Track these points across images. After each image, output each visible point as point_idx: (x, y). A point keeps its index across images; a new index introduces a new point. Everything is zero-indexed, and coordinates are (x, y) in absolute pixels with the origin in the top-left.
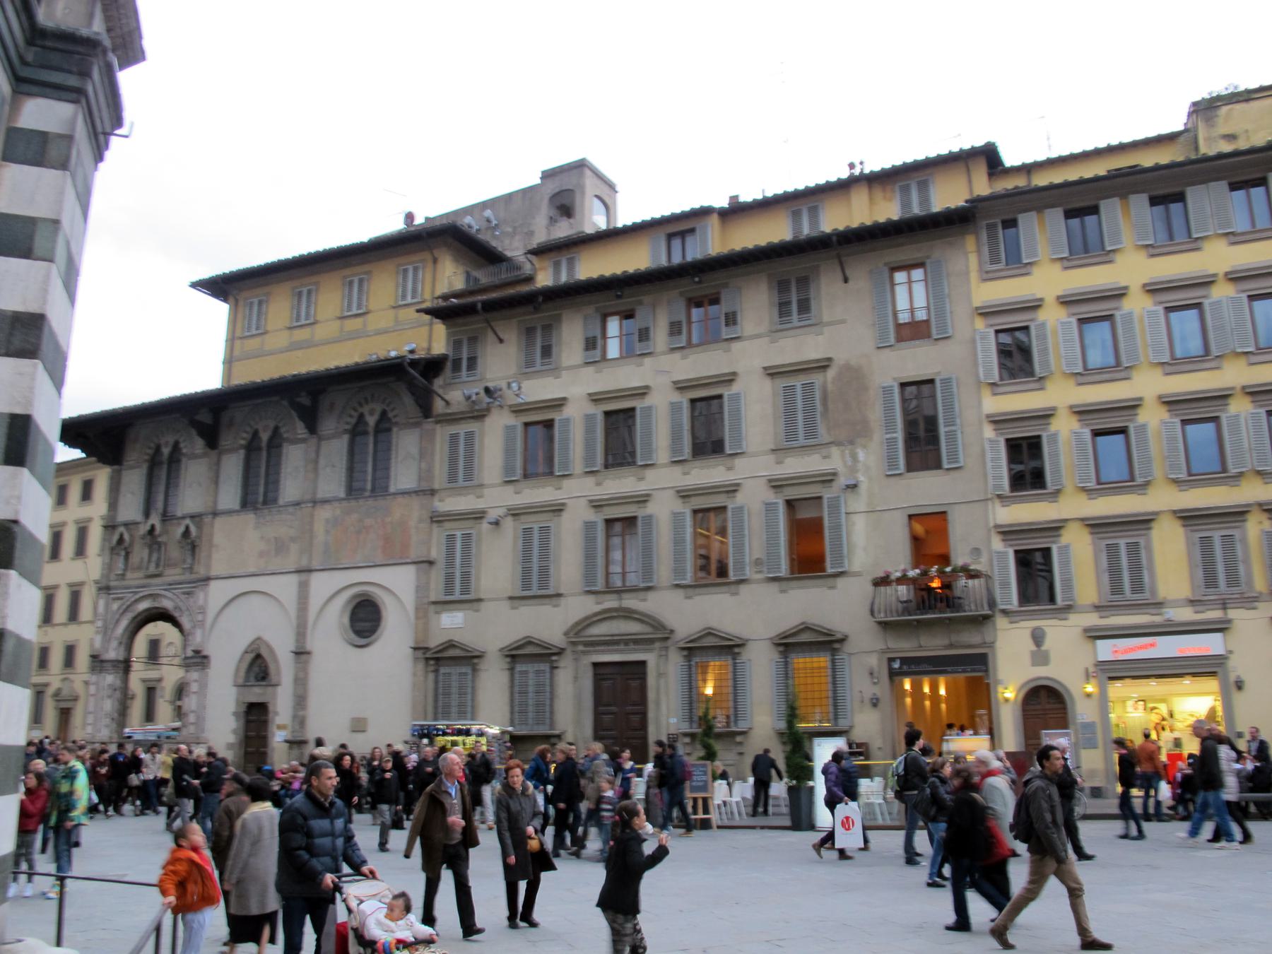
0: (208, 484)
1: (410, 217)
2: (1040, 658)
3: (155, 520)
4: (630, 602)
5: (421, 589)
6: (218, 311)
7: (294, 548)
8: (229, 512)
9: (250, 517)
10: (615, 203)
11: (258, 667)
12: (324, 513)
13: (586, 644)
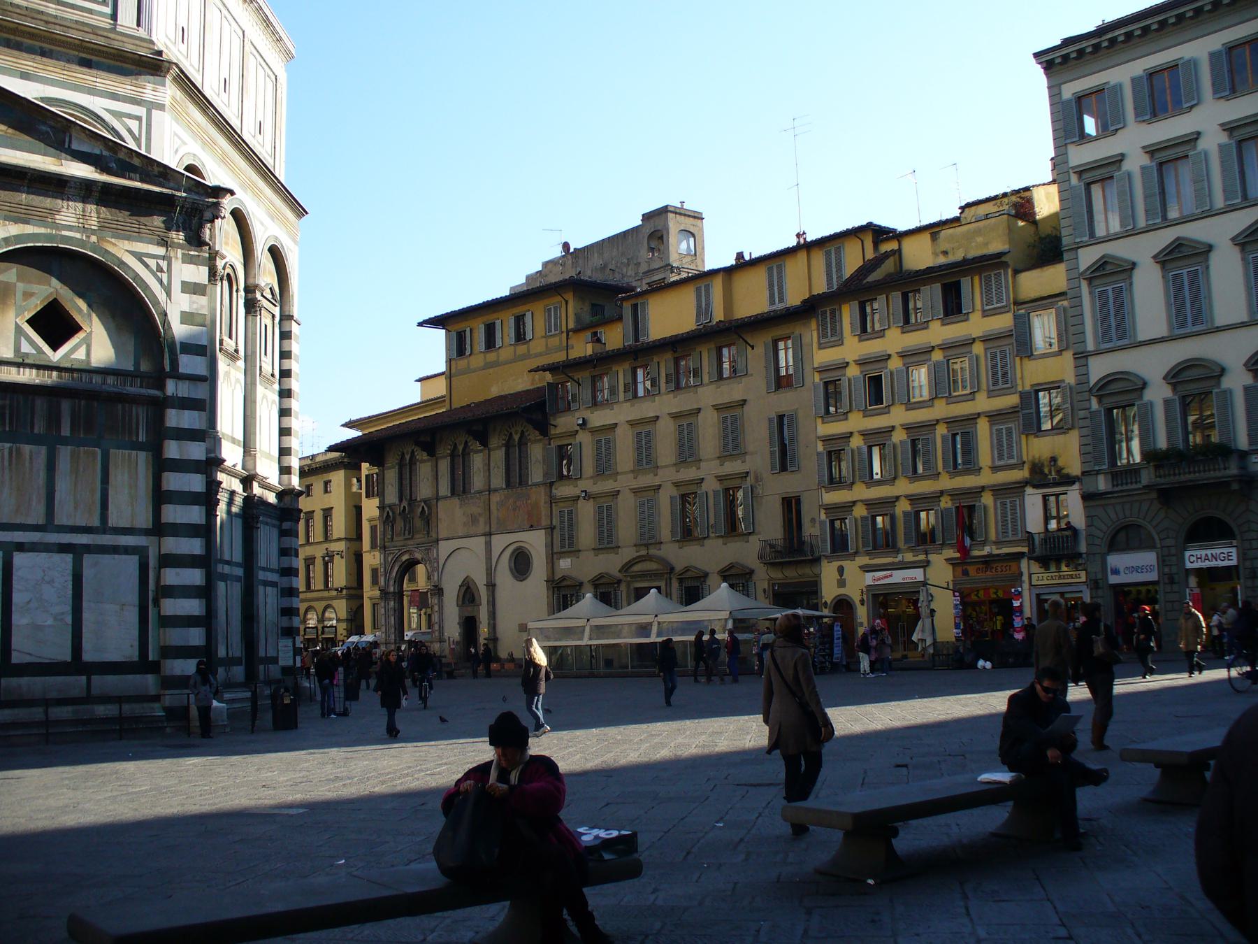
0: (430, 478)
1: (566, 246)
2: (842, 583)
3: (405, 503)
4: (653, 551)
5: (550, 545)
6: (439, 336)
7: (482, 520)
8: (445, 498)
9: (456, 501)
10: (701, 230)
11: (468, 594)
12: (495, 498)
13: (632, 577)
